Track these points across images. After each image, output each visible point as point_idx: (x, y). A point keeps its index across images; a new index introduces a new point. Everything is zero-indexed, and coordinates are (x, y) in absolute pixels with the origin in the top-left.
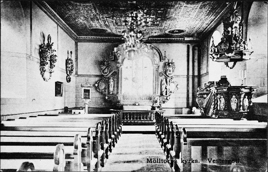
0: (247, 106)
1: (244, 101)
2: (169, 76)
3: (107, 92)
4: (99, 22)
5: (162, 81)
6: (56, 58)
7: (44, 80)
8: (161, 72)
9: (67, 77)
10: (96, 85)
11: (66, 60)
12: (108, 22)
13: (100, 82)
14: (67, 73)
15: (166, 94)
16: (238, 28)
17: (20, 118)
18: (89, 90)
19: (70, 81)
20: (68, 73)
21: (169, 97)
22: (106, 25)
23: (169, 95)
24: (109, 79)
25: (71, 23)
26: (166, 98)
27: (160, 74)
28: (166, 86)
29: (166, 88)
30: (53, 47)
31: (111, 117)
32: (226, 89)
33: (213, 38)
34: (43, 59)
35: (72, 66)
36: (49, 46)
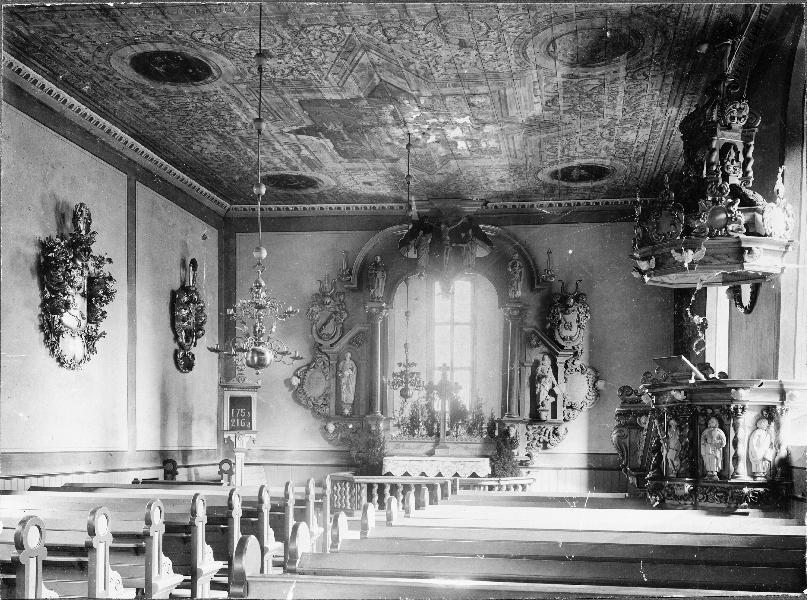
0: (764, 459)
1: (754, 441)
2: (562, 347)
3: (333, 407)
4: (274, 149)
5: (537, 364)
6: (111, 286)
7: (62, 364)
8: (534, 332)
9: (176, 352)
10: (296, 381)
11: (173, 293)
12: (307, 147)
13: (308, 369)
14: (176, 338)
15: (554, 416)
16: (740, 148)
17: (33, 489)
18: (250, 398)
19: (189, 366)
20: (182, 340)
21: (566, 424)
22: (306, 160)
23: (565, 420)
24: (340, 359)
25: (462, 126)
26: (554, 432)
27: (527, 342)
28: (553, 386)
29: (552, 393)
30: (96, 249)
31: (417, 507)
32: (683, 392)
33: (783, 175)
34: (53, 292)
35: (200, 311)
36: (79, 245)
